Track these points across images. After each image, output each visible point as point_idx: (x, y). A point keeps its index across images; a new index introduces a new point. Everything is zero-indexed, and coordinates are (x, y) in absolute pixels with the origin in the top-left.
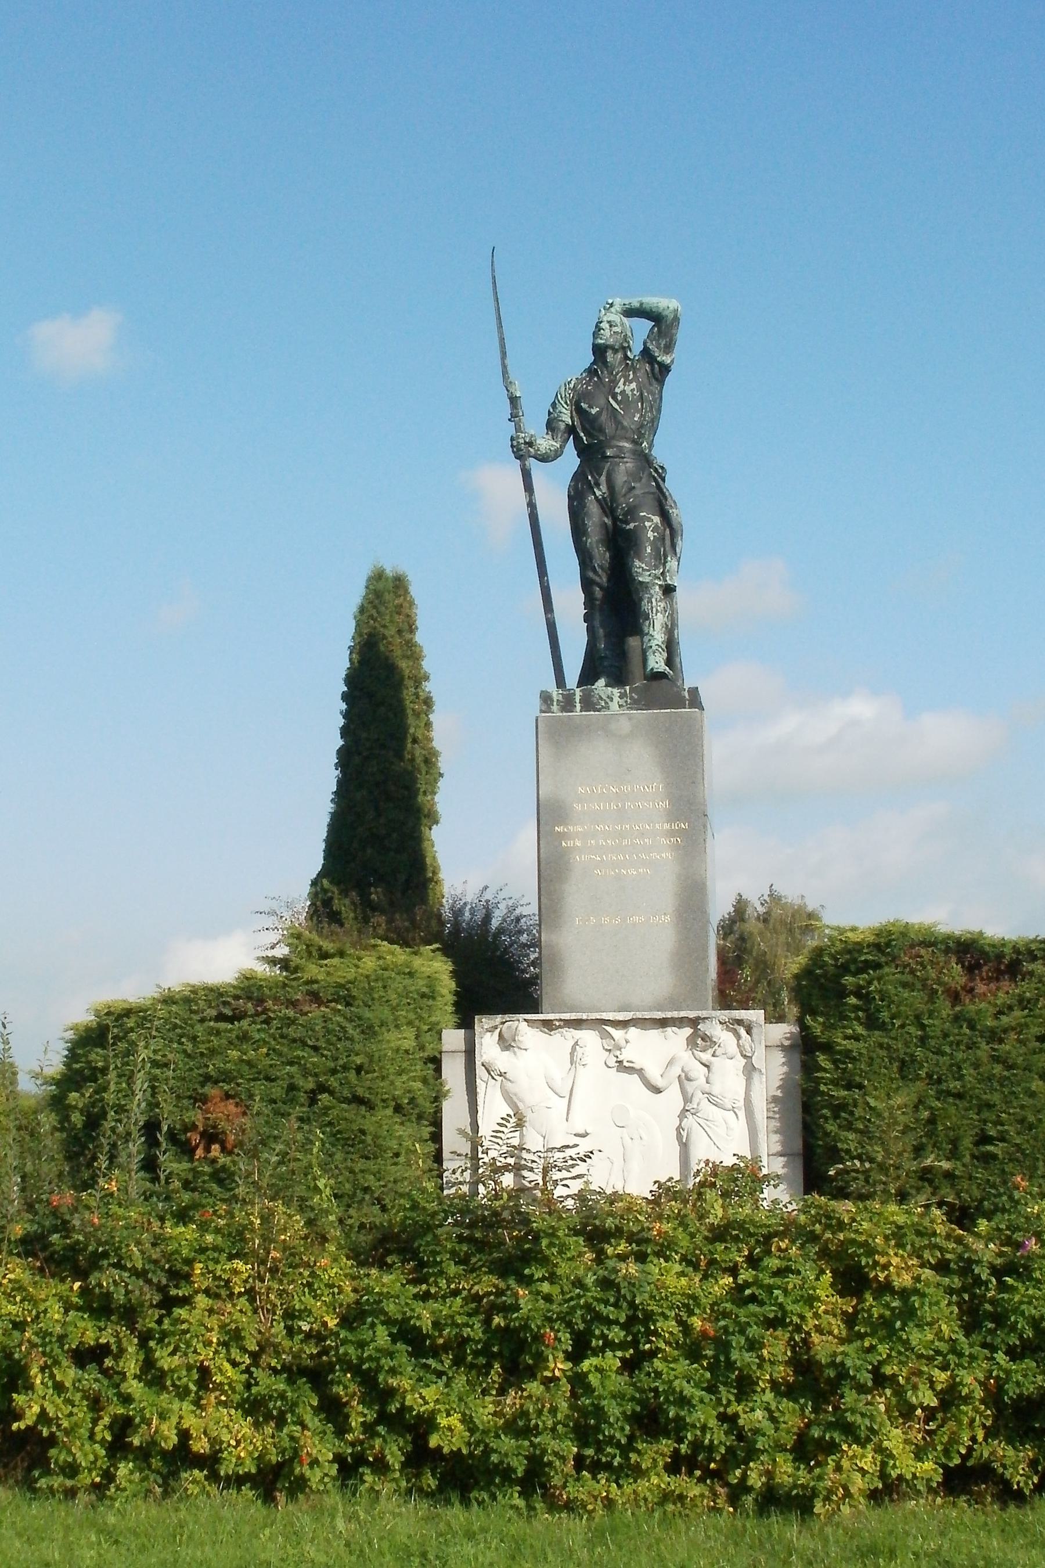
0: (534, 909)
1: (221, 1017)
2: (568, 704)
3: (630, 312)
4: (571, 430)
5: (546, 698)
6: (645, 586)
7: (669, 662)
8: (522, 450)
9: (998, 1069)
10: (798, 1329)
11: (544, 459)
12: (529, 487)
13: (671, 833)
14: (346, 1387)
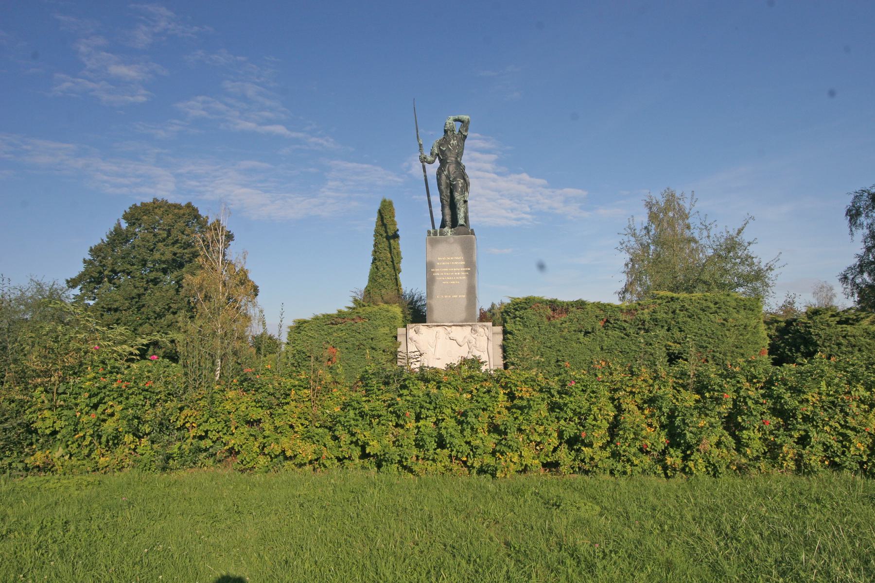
0: (425, 294)
1: (332, 324)
2: (435, 234)
3: (455, 120)
4: (438, 155)
5: (429, 232)
6: (459, 200)
7: (466, 222)
8: (423, 160)
9: (562, 340)
10: (492, 412)
11: (429, 163)
12: (425, 171)
13: (466, 271)
14: (340, 431)
